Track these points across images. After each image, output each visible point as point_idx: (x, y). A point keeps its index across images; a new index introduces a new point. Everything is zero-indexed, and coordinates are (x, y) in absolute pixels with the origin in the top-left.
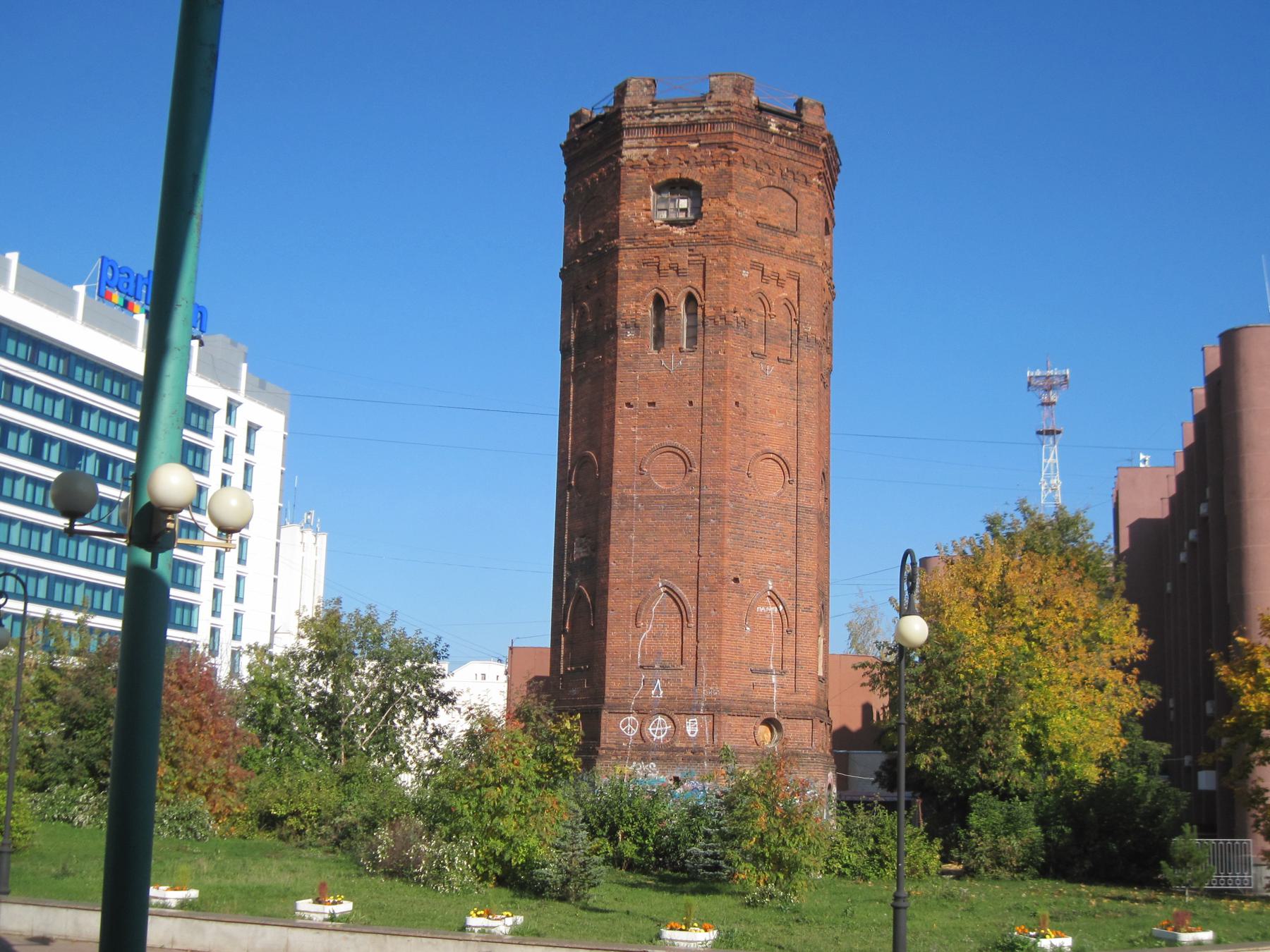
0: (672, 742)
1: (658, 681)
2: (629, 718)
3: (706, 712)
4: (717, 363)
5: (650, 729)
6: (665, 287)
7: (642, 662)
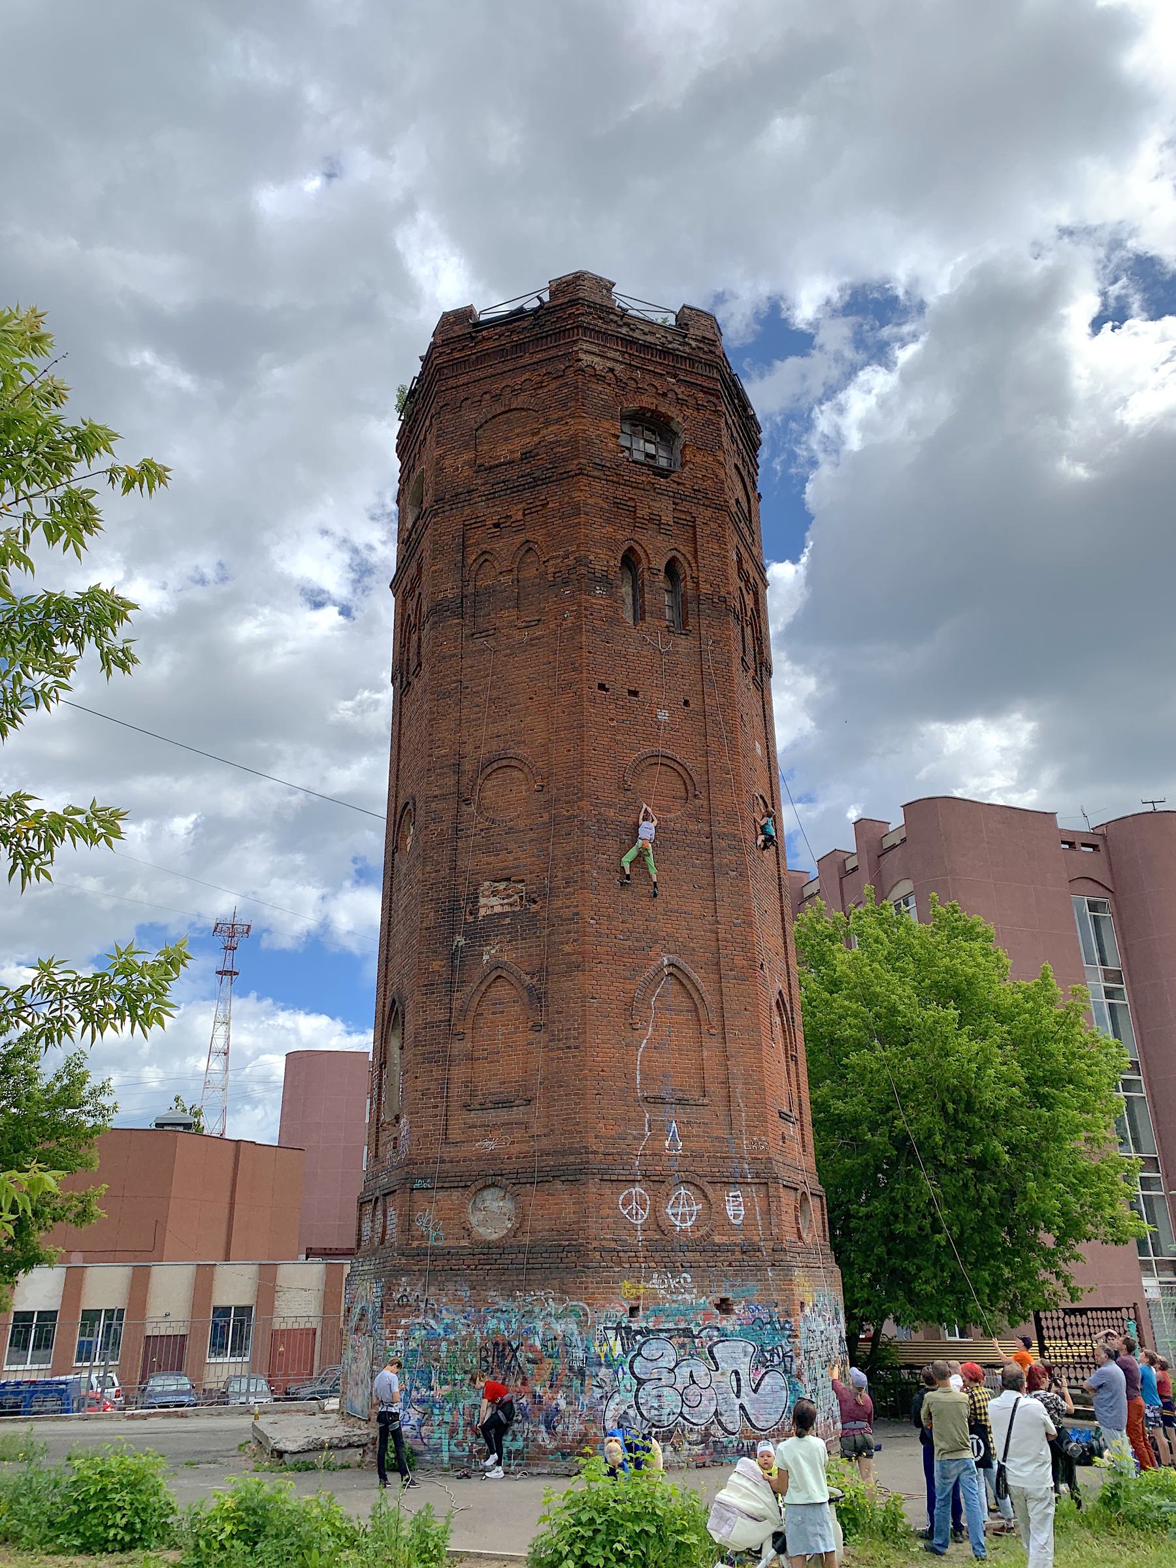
0: (708, 1235)
1: (674, 1125)
3: (757, 1180)
5: (669, 1211)
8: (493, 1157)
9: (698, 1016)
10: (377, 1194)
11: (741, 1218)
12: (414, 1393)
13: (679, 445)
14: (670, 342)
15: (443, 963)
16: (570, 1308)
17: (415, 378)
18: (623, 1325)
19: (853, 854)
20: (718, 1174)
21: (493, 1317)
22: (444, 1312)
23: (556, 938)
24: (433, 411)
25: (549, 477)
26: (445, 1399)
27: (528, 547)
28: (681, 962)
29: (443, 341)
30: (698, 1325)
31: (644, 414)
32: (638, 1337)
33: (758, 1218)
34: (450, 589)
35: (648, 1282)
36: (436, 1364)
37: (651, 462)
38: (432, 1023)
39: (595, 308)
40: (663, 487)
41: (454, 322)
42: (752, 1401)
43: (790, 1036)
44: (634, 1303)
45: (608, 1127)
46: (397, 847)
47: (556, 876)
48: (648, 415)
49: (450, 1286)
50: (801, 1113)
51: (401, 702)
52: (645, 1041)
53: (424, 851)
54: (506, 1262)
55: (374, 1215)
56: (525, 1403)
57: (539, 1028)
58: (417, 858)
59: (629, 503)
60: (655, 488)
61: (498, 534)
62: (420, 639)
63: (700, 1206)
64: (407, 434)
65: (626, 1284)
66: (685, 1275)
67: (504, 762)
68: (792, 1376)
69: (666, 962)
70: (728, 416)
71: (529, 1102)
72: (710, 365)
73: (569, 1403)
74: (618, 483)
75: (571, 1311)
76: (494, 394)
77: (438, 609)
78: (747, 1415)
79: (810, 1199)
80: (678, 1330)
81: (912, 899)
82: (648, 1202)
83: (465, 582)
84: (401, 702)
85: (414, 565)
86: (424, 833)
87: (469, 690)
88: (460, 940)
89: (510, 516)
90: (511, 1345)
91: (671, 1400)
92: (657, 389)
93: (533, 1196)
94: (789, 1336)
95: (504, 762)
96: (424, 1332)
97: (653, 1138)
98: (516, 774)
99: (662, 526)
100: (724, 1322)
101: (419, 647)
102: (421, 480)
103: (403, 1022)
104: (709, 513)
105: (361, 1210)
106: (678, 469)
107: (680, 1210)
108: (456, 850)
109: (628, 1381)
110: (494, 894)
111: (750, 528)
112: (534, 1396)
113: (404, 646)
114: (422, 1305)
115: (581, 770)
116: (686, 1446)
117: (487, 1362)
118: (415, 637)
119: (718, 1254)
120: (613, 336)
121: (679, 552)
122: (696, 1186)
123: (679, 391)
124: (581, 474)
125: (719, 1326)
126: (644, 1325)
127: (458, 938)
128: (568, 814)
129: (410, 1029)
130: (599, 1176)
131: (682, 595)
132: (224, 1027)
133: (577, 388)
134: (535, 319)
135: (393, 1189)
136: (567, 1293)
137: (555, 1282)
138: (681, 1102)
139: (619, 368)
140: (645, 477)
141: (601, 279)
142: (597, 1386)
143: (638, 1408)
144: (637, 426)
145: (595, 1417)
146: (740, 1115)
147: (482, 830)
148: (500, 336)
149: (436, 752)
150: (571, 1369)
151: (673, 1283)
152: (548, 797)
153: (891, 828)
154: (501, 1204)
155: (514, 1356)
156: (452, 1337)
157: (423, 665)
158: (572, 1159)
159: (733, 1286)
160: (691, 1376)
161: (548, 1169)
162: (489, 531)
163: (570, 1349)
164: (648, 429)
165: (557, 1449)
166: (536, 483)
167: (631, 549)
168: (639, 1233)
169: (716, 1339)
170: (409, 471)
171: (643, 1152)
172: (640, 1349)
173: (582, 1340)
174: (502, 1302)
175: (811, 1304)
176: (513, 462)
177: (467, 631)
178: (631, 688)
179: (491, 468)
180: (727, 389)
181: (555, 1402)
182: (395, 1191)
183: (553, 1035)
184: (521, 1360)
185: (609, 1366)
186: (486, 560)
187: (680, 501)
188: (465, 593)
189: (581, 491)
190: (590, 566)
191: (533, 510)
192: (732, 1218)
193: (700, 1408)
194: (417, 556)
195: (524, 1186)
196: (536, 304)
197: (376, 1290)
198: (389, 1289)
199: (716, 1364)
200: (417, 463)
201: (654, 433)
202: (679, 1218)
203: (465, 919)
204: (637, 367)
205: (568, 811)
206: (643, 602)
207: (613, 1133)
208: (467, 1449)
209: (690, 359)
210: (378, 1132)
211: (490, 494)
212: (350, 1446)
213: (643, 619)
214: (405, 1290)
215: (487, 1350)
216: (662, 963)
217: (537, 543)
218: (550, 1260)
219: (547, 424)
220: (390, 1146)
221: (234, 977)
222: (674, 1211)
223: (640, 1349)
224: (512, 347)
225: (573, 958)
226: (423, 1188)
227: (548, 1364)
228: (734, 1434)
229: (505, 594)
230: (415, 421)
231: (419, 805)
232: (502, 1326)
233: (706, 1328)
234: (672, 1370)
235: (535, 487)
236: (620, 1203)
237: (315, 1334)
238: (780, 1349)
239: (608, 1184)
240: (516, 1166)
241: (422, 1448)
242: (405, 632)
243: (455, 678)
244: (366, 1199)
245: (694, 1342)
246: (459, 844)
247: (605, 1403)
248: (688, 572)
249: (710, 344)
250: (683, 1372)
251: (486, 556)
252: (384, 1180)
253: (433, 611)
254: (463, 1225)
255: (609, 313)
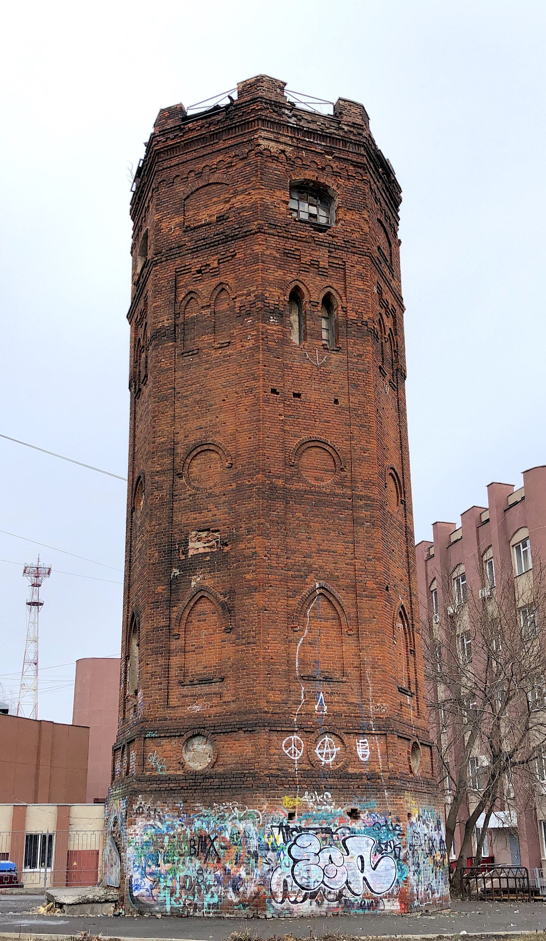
0: (344, 767)
1: (321, 694)
2: (292, 738)
3: (379, 732)
4: (361, 367)
5: (317, 751)
6: (307, 280)
7: (300, 672)
8: (199, 716)
9: (340, 623)
10: (124, 743)
11: (367, 757)
12: (147, 869)
13: (334, 206)
14: (328, 128)
15: (164, 587)
16: (248, 813)
17: (141, 160)
18: (284, 825)
19: (487, 509)
20: (351, 728)
21: (198, 820)
22: (166, 817)
23: (241, 570)
24: (153, 186)
25: (237, 235)
26: (167, 873)
27: (221, 288)
28: (329, 586)
29: (160, 132)
30: (336, 826)
31: (307, 184)
32: (294, 833)
33: (379, 757)
34: (166, 321)
35: (301, 797)
36: (161, 850)
37: (314, 220)
38: (158, 628)
39: (271, 105)
40: (320, 240)
41: (168, 117)
42: (372, 876)
43: (410, 637)
44: (292, 811)
45: (275, 696)
46: (134, 508)
47: (241, 527)
48: (311, 184)
49: (170, 800)
50: (417, 690)
51: (135, 403)
52: (302, 639)
53: (151, 510)
54: (207, 784)
55: (122, 757)
56: (219, 874)
57: (229, 631)
58: (146, 515)
59: (295, 253)
60: (315, 241)
61: (200, 278)
62: (146, 357)
63: (339, 749)
64: (137, 201)
65: (287, 798)
66: (326, 793)
67: (205, 447)
68: (400, 860)
69: (317, 586)
70: (372, 183)
71: (222, 679)
72: (358, 144)
73: (248, 874)
74: (287, 238)
75: (249, 815)
76: (197, 172)
77: (158, 335)
78: (368, 884)
79: (420, 747)
80: (322, 828)
81: (528, 542)
82: (303, 745)
83: (176, 315)
84: (135, 403)
85: (142, 301)
86: (150, 498)
87: (180, 395)
88: (176, 572)
89: (209, 265)
90: (210, 838)
91: (316, 874)
92: (318, 165)
93: (224, 742)
94: (399, 834)
95: (205, 447)
96: (153, 830)
97: (307, 703)
98: (214, 455)
99: (320, 269)
100: (354, 824)
101: (146, 362)
102: (146, 237)
103: (139, 627)
104: (355, 258)
105: (114, 755)
106: (334, 225)
107: (325, 751)
108: (172, 509)
109: (287, 860)
110: (199, 540)
111: (390, 268)
112: (225, 870)
113: (137, 362)
114: (152, 813)
115: (258, 452)
116: (326, 901)
117: (195, 848)
118: (143, 355)
119: (350, 780)
120: (285, 125)
121: (333, 288)
122: (337, 735)
123: (334, 165)
124: (260, 232)
125: (350, 826)
126: (298, 825)
127: (175, 570)
128: (249, 483)
129: (143, 632)
130: (269, 728)
131: (335, 321)
132: (34, 643)
133: (257, 166)
134: (227, 114)
135: (133, 738)
136: (245, 803)
137: (239, 796)
138: (327, 679)
139: (289, 149)
140: (308, 232)
141: (276, 80)
142: (266, 863)
143: (294, 878)
144: (303, 193)
145: (265, 882)
146: (368, 689)
147: (190, 496)
148: (201, 127)
149: (158, 440)
150: (249, 852)
151: (319, 798)
152: (235, 471)
153: (515, 489)
154: (204, 747)
155: (212, 845)
156: (172, 833)
157: (149, 376)
158: (251, 716)
159: (361, 801)
160: (330, 858)
161: (235, 723)
162: (194, 276)
163: (248, 840)
164: (311, 195)
165: (240, 902)
166: (227, 239)
167: (297, 287)
168: (296, 765)
169: (347, 835)
170: (139, 230)
171: (299, 712)
172: (295, 840)
173: (256, 834)
174: (204, 810)
175: (417, 816)
176: (211, 224)
177: (178, 352)
178: (295, 392)
179: (195, 228)
180: (372, 162)
181: (238, 873)
182: (134, 739)
183: (238, 635)
184: (217, 847)
185: (274, 850)
186: (192, 298)
187: (334, 250)
188: (177, 322)
189: (260, 244)
190: (266, 301)
191: (225, 260)
192: (360, 757)
193: (336, 879)
194: (144, 295)
195: (219, 734)
196: (228, 101)
197: (123, 804)
198: (130, 804)
199: (347, 851)
200: (144, 224)
201: (316, 198)
202: (324, 756)
203: (180, 557)
204: (302, 148)
205: (249, 481)
206: (306, 326)
207: (279, 699)
208: (182, 903)
209: (343, 140)
210: (125, 703)
211: (203, 245)
212: (107, 901)
213: (305, 340)
214: (141, 803)
215: (194, 841)
216: (315, 586)
217: (227, 285)
218: (236, 783)
219: (236, 194)
220: (132, 711)
221: (40, 607)
222: (321, 751)
223: (295, 840)
224: (210, 135)
225: (252, 583)
226: (152, 737)
227: (234, 850)
228: (359, 895)
229: (205, 323)
230: (142, 192)
231: (147, 478)
232: (204, 826)
233: (340, 828)
234: (317, 854)
235: (226, 242)
236: (283, 745)
237: (98, 854)
238: (392, 842)
239: (275, 734)
240: (214, 722)
241: (153, 902)
242: (137, 351)
243: (170, 386)
244: (117, 747)
245: (332, 837)
246: (175, 506)
247: (271, 873)
248: (339, 303)
249: (358, 128)
250: (325, 855)
251: (192, 295)
252: (128, 734)
253: (154, 337)
254: (179, 761)
255: (281, 108)
